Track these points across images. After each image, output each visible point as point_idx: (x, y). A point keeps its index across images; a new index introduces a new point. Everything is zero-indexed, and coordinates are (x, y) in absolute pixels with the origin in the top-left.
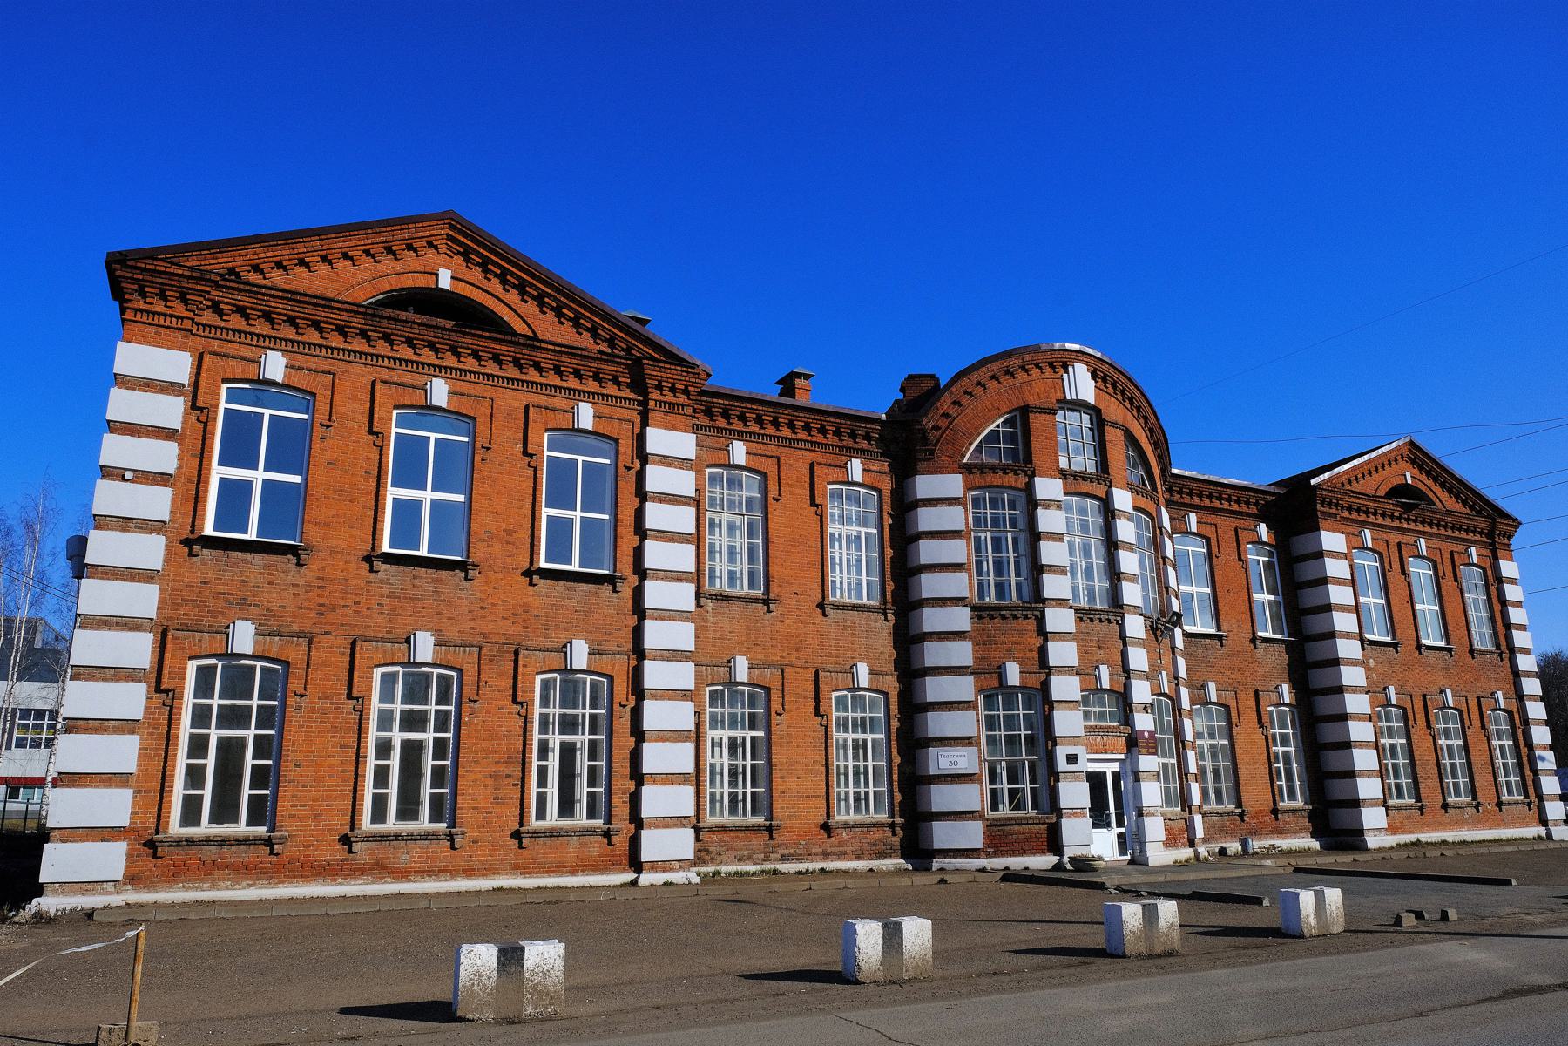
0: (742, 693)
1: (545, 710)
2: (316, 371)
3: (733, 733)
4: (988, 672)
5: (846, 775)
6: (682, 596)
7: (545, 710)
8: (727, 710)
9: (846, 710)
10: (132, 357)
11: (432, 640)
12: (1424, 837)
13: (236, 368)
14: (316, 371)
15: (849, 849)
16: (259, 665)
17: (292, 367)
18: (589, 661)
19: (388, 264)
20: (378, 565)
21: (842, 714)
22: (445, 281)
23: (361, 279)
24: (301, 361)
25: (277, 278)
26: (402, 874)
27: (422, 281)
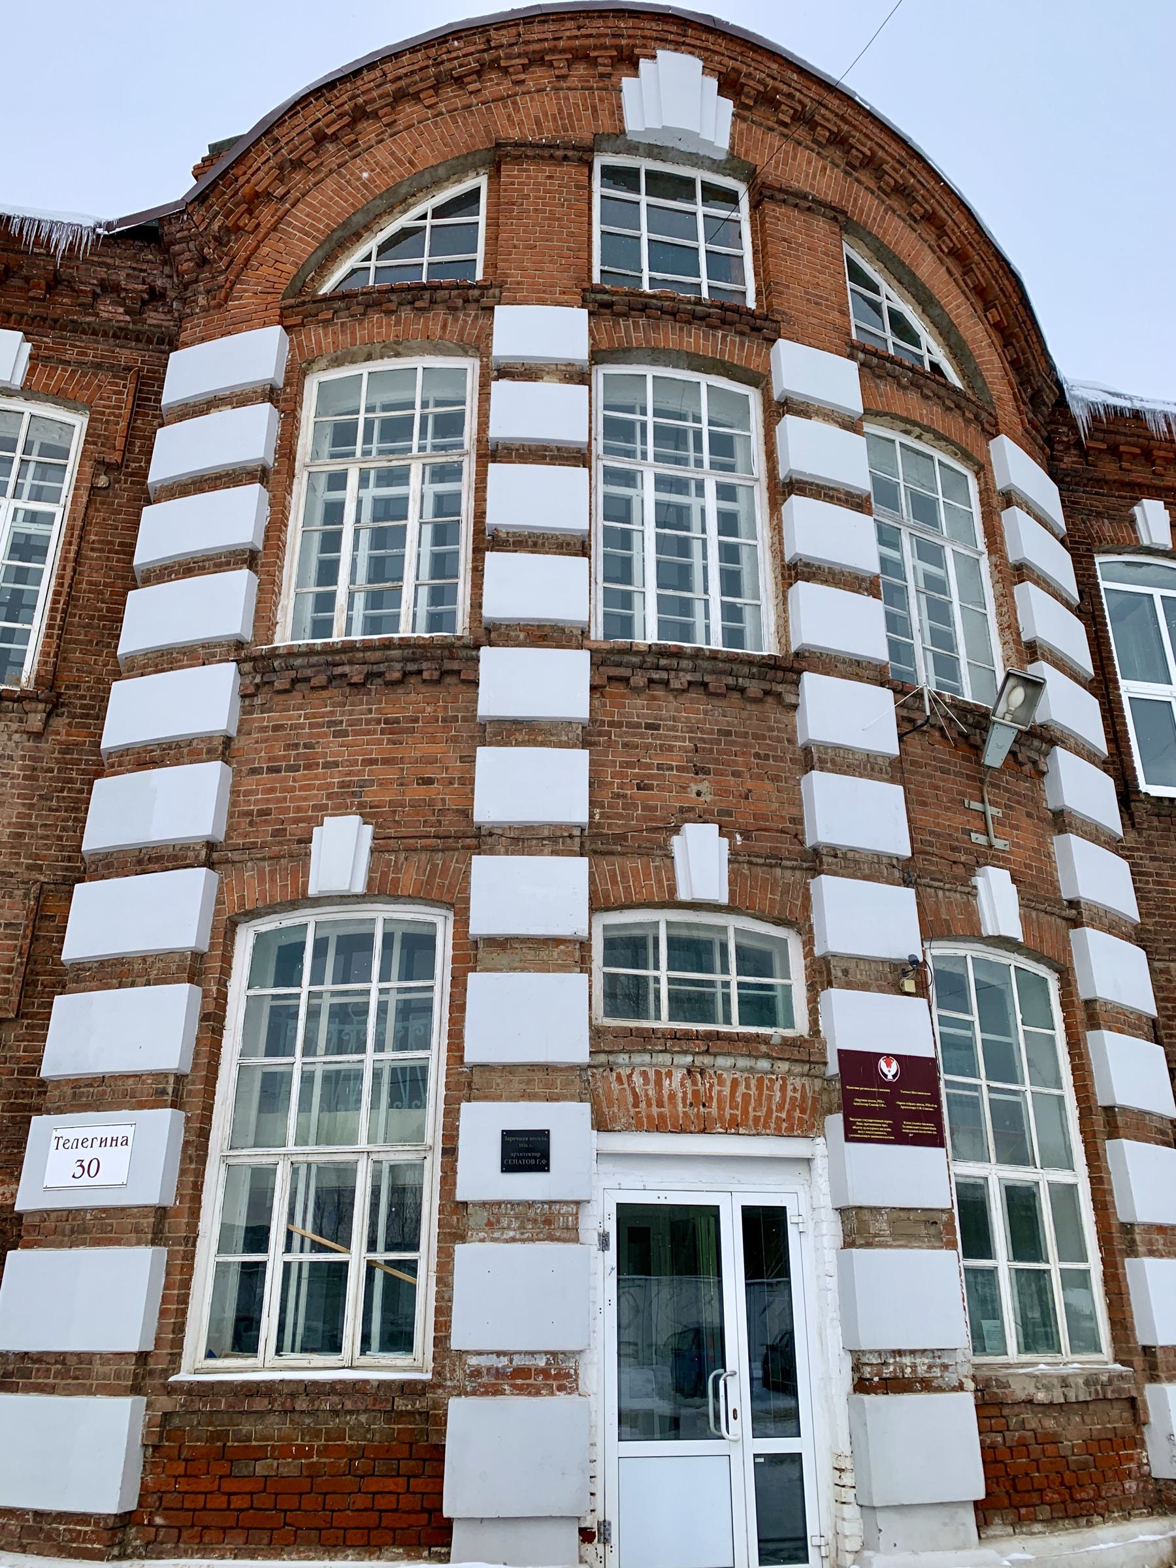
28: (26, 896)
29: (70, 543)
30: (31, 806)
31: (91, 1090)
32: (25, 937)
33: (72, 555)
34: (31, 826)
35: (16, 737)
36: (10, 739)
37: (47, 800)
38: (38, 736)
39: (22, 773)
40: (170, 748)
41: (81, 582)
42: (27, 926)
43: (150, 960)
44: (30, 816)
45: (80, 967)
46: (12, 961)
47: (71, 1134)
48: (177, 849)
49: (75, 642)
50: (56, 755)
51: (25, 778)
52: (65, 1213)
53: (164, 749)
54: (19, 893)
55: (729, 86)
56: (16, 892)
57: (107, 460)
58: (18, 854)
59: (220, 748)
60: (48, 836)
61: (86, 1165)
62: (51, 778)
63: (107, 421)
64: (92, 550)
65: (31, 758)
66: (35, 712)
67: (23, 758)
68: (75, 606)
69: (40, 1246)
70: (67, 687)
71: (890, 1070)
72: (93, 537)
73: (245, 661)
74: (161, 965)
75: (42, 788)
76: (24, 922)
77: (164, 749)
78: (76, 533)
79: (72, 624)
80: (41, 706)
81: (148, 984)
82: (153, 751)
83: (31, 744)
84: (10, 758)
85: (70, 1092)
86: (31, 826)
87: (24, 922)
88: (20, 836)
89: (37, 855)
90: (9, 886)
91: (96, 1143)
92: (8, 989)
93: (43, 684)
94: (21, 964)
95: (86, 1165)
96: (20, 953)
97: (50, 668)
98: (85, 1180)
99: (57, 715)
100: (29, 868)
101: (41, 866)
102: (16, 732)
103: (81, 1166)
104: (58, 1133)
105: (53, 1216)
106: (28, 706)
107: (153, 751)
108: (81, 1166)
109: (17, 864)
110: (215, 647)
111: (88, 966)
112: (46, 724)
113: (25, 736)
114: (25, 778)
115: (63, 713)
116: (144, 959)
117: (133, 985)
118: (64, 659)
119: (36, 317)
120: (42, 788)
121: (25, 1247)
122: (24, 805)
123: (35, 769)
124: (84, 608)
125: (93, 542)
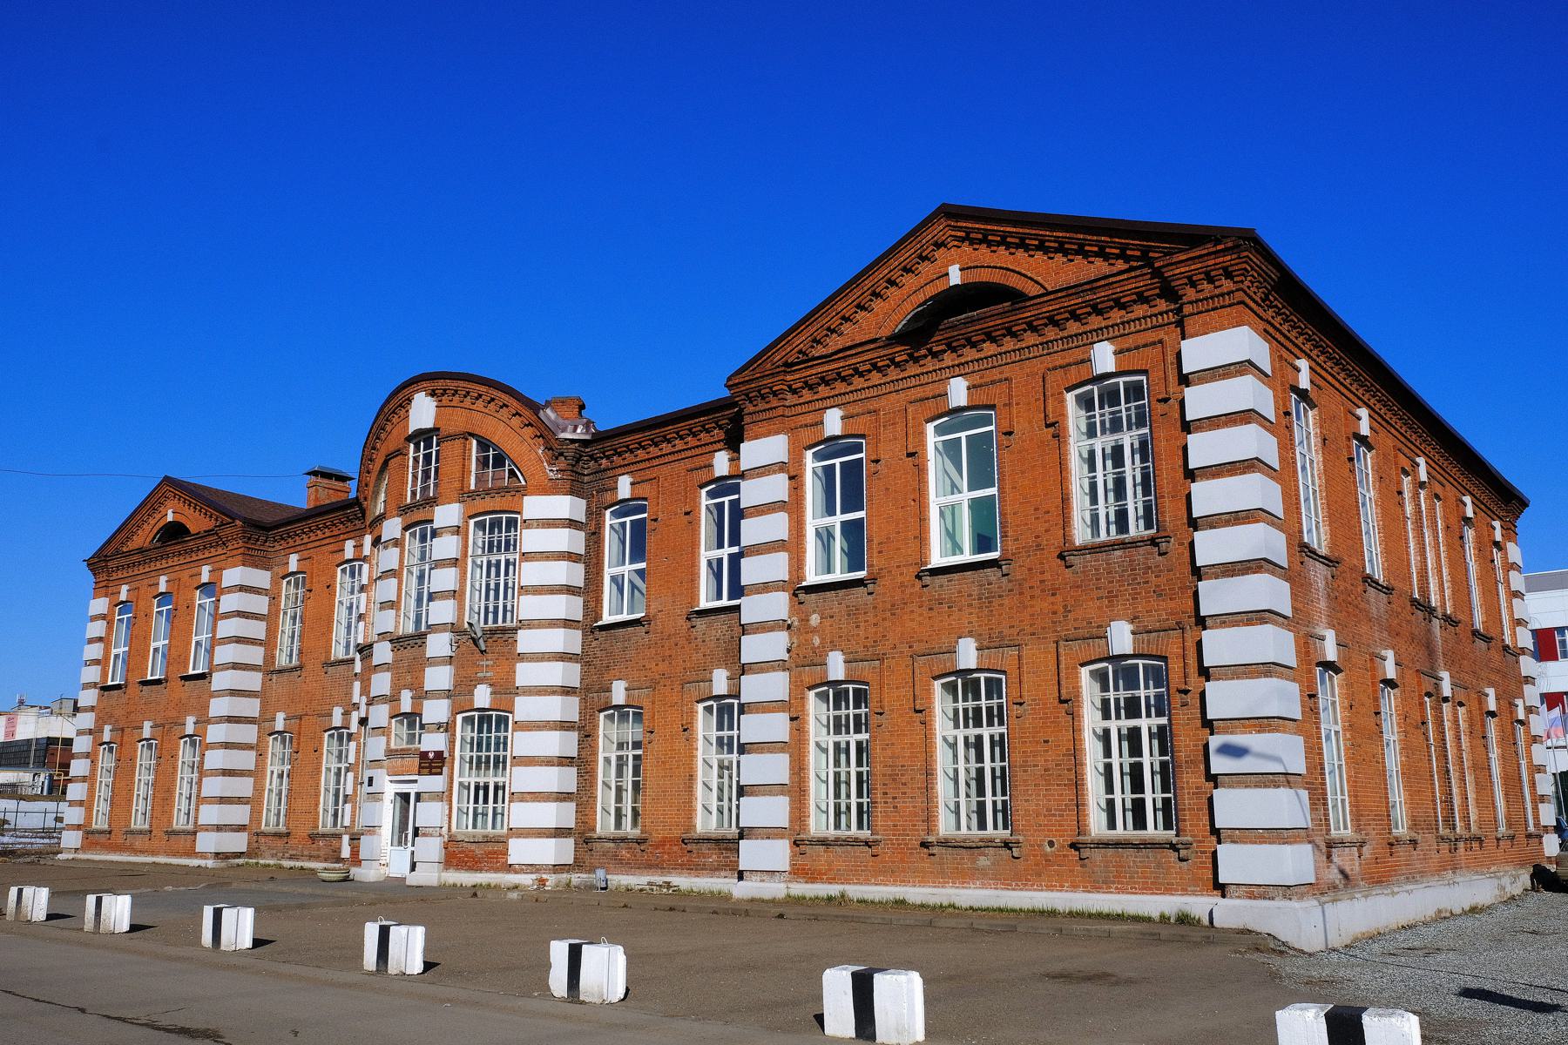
0: (847, 691)
1: (837, 713)
2: (1137, 348)
3: (838, 738)
4: (459, 694)
5: (848, 784)
6: (777, 606)
7: (837, 713)
8: (852, 711)
9: (977, 697)
10: (1198, 352)
11: (489, 690)
12: (855, 891)
13: (1074, 375)
14: (1137, 348)
15: (322, 853)
16: (1140, 662)
17: (974, 386)
18: (847, 669)
19: (909, 281)
20: (927, 580)
21: (971, 704)
22: (955, 277)
23: (892, 312)
24: (1130, 342)
25: (835, 342)
26: (136, 852)
27: (940, 286)
55: (433, 394)
71: (431, 755)
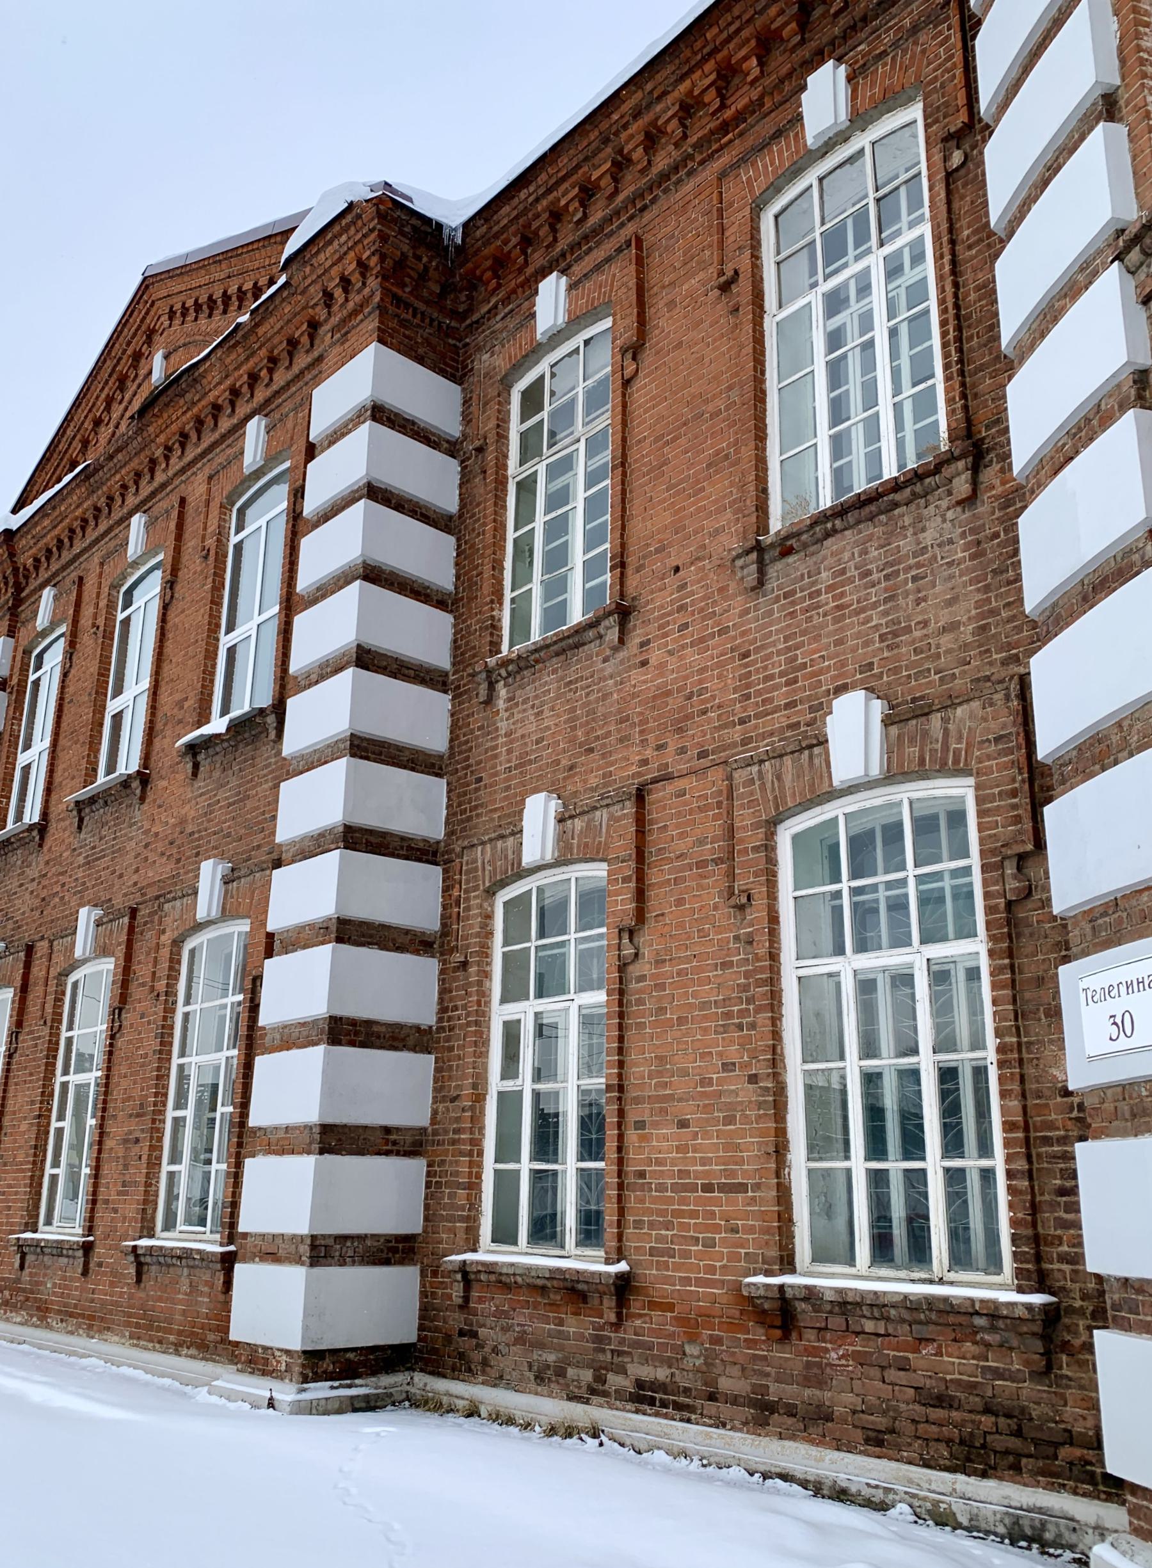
28: (1007, 698)
29: (942, 257)
30: (987, 589)
31: (1107, 919)
32: (1019, 747)
33: (947, 268)
34: (993, 612)
35: (950, 515)
36: (944, 521)
37: (1002, 572)
38: (970, 501)
39: (966, 554)
40: (1080, 430)
41: (967, 294)
42: (1018, 734)
43: (1125, 724)
44: (988, 600)
45: (1062, 761)
46: (1014, 780)
47: (1096, 982)
48: (1119, 559)
49: (981, 368)
50: (998, 514)
51: (973, 557)
52: (1120, 1089)
53: (1075, 435)
54: (999, 697)
56: (996, 697)
57: (952, 130)
58: (988, 651)
59: (1133, 392)
60: (1014, 616)
61: (1118, 1020)
62: (999, 545)
63: (943, 86)
64: (970, 247)
65: (973, 531)
66: (959, 474)
67: (963, 535)
68: (969, 327)
69: (1107, 1136)
70: (988, 428)
72: (966, 233)
73: (1128, 249)
74: (1139, 725)
75: (992, 561)
76: (1014, 730)
77: (1075, 435)
78: (945, 239)
79: (971, 350)
80: (961, 464)
81: (1131, 755)
82: (1064, 445)
83: (968, 514)
84: (951, 542)
85: (1088, 928)
86: (993, 612)
87: (1014, 730)
88: (984, 628)
89: (1009, 644)
90: (985, 692)
91: (1123, 989)
92: (1019, 816)
93: (957, 439)
94: (1023, 781)
95: (1118, 1020)
96: (1020, 769)
97: (960, 415)
98: (1123, 1043)
99: (986, 466)
100: (1004, 663)
101: (1017, 655)
102: (949, 509)
103: (1115, 1023)
104: (1083, 985)
105: (1109, 1092)
106: (947, 471)
107: (1064, 445)
108: (1115, 1023)
109: (991, 664)
110: (1094, 259)
111: (1067, 758)
112: (975, 483)
113: (959, 509)
114: (973, 557)
115: (991, 461)
116: (1119, 725)
117: (1116, 763)
118: (976, 396)
119: (845, 32)
120: (992, 561)
121: (1095, 1138)
122: (978, 590)
123: (979, 543)
124: (979, 321)
125: (968, 237)
